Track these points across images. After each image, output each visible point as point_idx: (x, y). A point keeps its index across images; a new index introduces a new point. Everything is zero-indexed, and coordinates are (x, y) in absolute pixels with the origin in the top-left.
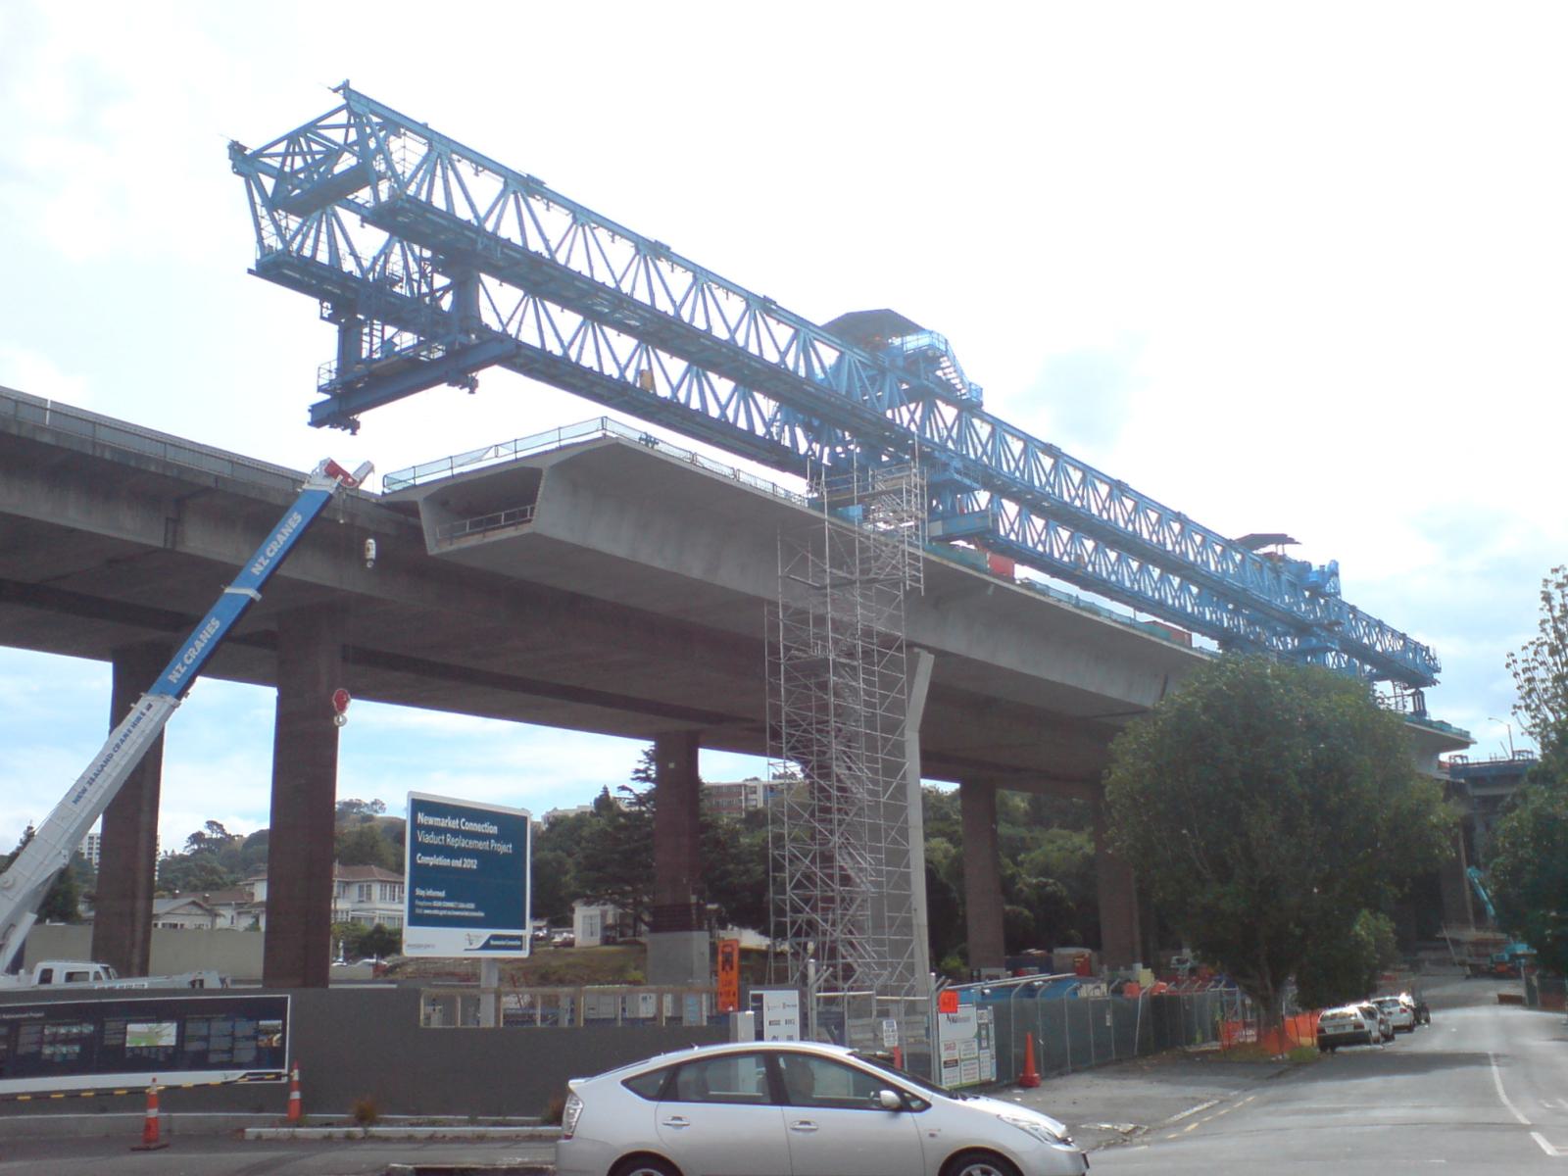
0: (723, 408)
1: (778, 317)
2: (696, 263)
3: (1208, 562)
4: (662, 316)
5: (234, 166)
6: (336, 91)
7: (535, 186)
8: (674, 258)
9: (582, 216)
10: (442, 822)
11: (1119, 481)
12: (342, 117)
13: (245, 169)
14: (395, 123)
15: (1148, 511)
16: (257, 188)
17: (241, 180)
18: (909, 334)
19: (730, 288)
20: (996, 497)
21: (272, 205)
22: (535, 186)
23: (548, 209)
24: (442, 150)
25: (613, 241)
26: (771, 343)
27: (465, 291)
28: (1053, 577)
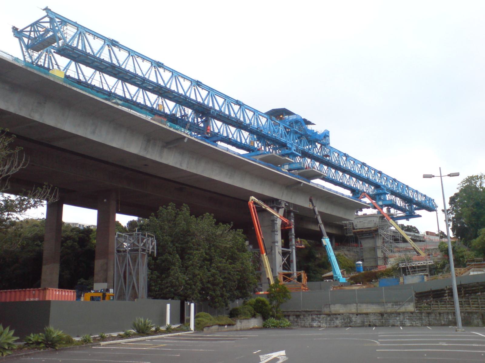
0: (233, 135)
1: (202, 87)
2: (152, 59)
3: (376, 179)
4: (199, 103)
5: (14, 35)
6: (44, 10)
7: (115, 43)
8: (165, 67)
9: (131, 53)
10: (366, 237)
11: (238, 100)
12: (47, 19)
13: (18, 36)
14: (65, 22)
15: (334, 153)
16: (23, 43)
17: (17, 39)
18: (291, 115)
19: (185, 78)
20: (351, 177)
21: (28, 47)
22: (115, 43)
23: (164, 72)
24: (82, 31)
25: (184, 81)
26: (248, 117)
27: (206, 122)
28: (228, 144)
